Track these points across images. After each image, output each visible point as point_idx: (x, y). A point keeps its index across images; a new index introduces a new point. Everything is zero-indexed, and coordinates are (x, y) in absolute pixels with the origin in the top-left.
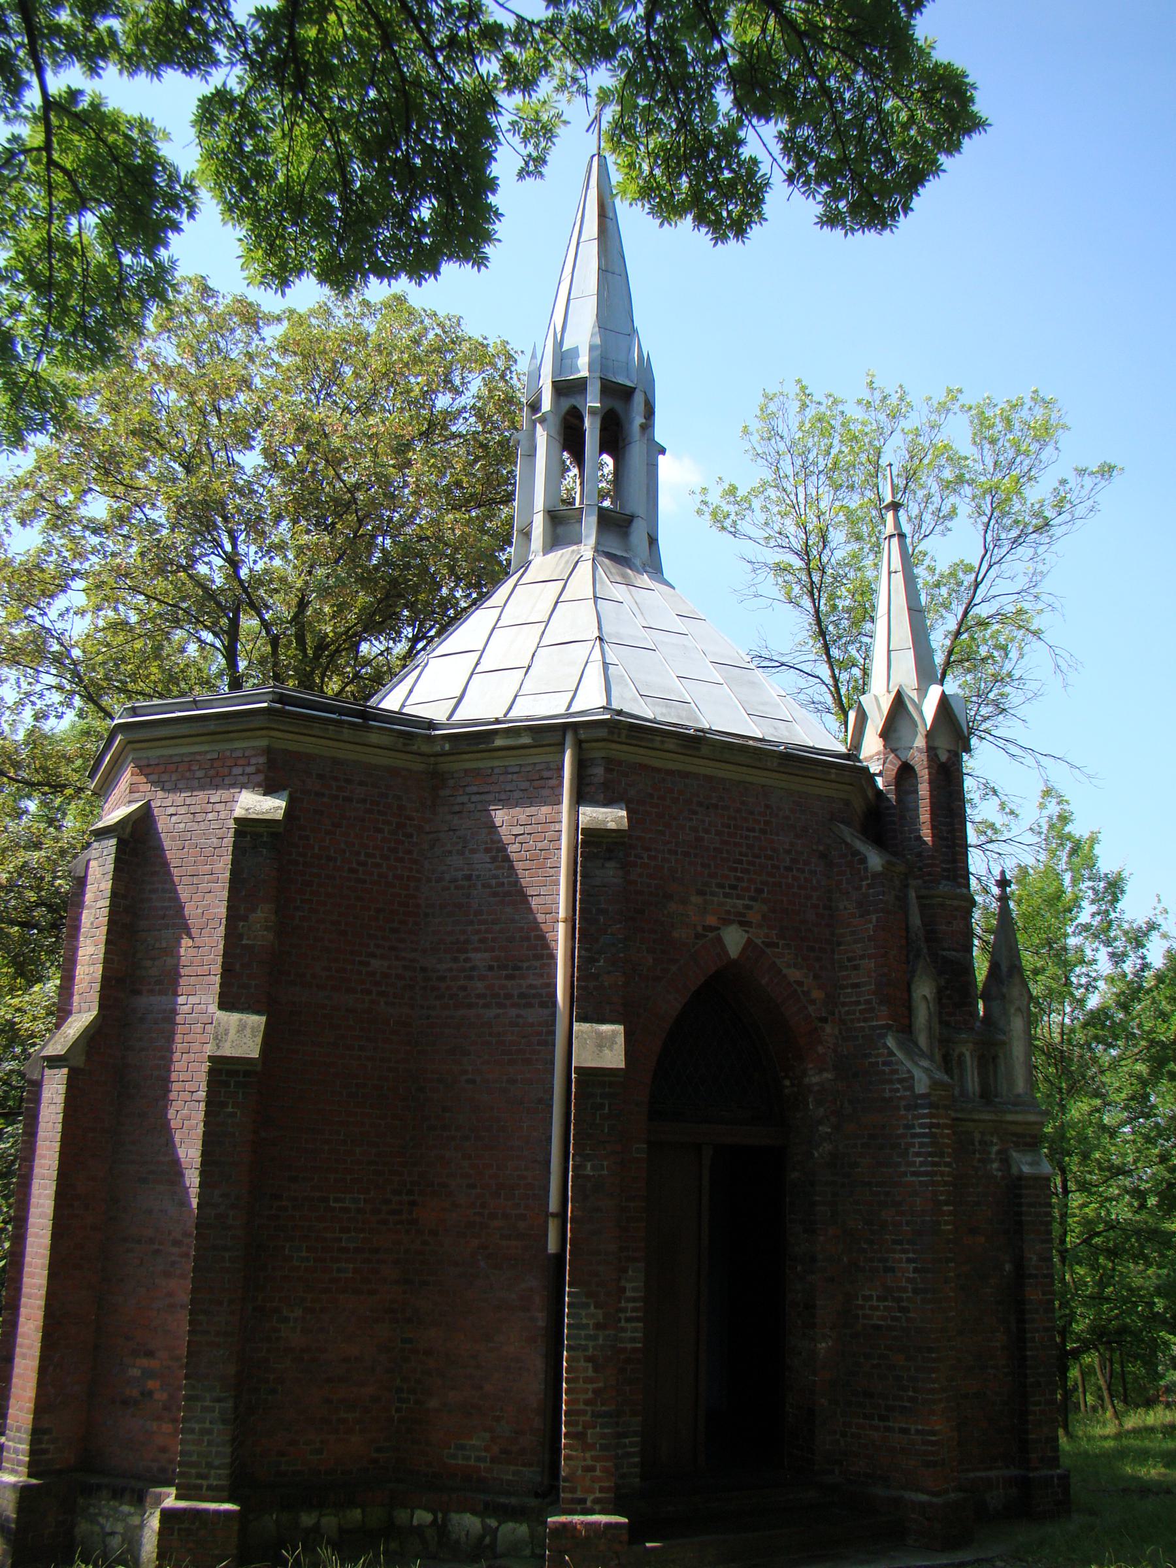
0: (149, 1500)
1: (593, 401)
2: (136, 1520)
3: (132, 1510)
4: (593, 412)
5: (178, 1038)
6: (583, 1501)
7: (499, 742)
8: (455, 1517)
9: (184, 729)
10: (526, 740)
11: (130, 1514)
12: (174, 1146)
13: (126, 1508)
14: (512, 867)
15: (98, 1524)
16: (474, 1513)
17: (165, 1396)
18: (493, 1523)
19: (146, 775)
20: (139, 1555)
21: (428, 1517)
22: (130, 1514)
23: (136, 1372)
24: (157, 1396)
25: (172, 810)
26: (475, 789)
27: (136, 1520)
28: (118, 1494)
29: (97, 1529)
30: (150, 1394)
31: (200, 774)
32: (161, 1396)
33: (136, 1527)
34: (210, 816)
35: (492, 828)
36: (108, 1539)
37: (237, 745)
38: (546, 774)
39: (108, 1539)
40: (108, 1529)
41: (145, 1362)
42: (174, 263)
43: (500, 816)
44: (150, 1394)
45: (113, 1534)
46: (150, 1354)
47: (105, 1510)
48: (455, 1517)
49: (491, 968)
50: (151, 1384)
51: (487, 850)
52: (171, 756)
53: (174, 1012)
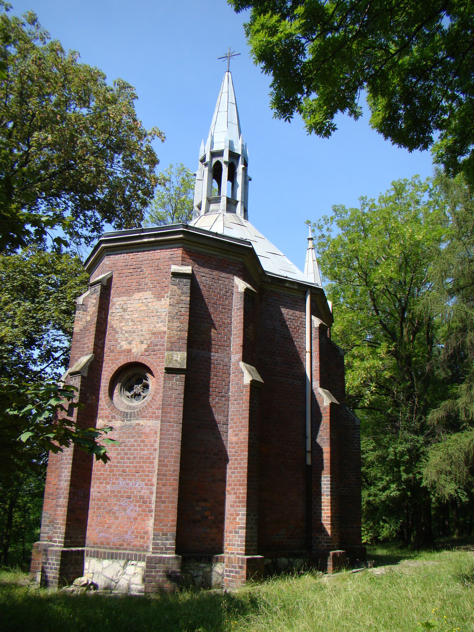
0: (214, 560)
1: (226, 158)
2: (208, 569)
3: (206, 565)
4: (225, 163)
5: (212, 369)
6: (334, 546)
7: (287, 285)
8: (279, 560)
9: (205, 242)
10: (296, 287)
11: (205, 567)
12: (213, 414)
13: (202, 565)
14: (288, 330)
15: (190, 573)
16: (285, 557)
17: (213, 517)
18: (291, 560)
19: (189, 256)
20: (211, 583)
21: (270, 561)
22: (205, 567)
23: (199, 509)
24: (209, 518)
25: (203, 274)
26: (275, 298)
27: (208, 569)
28: (199, 560)
29: (189, 575)
30: (206, 517)
31: (214, 263)
32: (211, 518)
33: (209, 572)
34: (220, 282)
35: (281, 314)
36: (195, 579)
37: (230, 257)
38: (298, 300)
39: (195, 579)
40: (195, 575)
41: (203, 504)
42: (255, 63)
43: (284, 310)
44: (206, 517)
45: (197, 576)
46: (205, 500)
47: (193, 567)
48: (279, 560)
49: (282, 363)
50: (206, 513)
51: (280, 321)
52: (201, 252)
53: (210, 358)
